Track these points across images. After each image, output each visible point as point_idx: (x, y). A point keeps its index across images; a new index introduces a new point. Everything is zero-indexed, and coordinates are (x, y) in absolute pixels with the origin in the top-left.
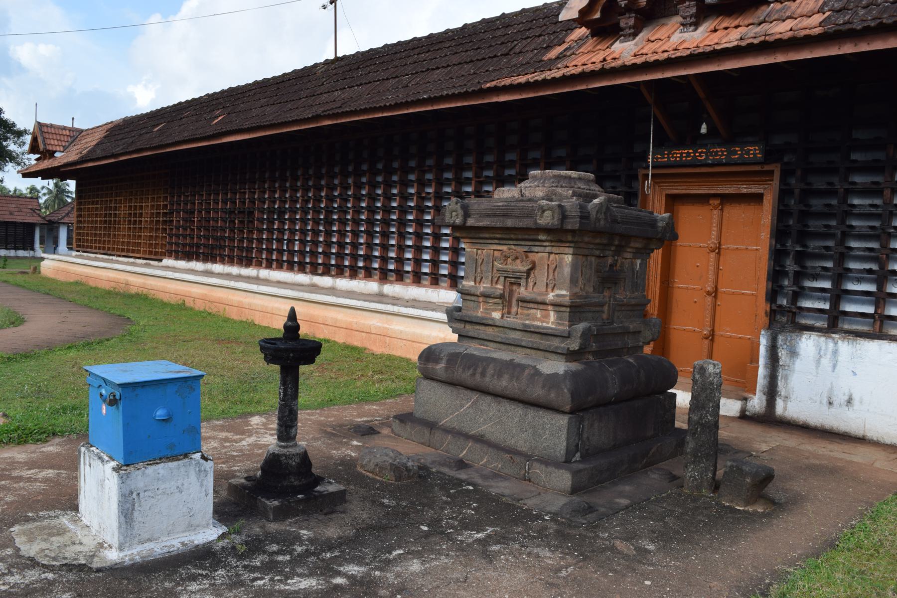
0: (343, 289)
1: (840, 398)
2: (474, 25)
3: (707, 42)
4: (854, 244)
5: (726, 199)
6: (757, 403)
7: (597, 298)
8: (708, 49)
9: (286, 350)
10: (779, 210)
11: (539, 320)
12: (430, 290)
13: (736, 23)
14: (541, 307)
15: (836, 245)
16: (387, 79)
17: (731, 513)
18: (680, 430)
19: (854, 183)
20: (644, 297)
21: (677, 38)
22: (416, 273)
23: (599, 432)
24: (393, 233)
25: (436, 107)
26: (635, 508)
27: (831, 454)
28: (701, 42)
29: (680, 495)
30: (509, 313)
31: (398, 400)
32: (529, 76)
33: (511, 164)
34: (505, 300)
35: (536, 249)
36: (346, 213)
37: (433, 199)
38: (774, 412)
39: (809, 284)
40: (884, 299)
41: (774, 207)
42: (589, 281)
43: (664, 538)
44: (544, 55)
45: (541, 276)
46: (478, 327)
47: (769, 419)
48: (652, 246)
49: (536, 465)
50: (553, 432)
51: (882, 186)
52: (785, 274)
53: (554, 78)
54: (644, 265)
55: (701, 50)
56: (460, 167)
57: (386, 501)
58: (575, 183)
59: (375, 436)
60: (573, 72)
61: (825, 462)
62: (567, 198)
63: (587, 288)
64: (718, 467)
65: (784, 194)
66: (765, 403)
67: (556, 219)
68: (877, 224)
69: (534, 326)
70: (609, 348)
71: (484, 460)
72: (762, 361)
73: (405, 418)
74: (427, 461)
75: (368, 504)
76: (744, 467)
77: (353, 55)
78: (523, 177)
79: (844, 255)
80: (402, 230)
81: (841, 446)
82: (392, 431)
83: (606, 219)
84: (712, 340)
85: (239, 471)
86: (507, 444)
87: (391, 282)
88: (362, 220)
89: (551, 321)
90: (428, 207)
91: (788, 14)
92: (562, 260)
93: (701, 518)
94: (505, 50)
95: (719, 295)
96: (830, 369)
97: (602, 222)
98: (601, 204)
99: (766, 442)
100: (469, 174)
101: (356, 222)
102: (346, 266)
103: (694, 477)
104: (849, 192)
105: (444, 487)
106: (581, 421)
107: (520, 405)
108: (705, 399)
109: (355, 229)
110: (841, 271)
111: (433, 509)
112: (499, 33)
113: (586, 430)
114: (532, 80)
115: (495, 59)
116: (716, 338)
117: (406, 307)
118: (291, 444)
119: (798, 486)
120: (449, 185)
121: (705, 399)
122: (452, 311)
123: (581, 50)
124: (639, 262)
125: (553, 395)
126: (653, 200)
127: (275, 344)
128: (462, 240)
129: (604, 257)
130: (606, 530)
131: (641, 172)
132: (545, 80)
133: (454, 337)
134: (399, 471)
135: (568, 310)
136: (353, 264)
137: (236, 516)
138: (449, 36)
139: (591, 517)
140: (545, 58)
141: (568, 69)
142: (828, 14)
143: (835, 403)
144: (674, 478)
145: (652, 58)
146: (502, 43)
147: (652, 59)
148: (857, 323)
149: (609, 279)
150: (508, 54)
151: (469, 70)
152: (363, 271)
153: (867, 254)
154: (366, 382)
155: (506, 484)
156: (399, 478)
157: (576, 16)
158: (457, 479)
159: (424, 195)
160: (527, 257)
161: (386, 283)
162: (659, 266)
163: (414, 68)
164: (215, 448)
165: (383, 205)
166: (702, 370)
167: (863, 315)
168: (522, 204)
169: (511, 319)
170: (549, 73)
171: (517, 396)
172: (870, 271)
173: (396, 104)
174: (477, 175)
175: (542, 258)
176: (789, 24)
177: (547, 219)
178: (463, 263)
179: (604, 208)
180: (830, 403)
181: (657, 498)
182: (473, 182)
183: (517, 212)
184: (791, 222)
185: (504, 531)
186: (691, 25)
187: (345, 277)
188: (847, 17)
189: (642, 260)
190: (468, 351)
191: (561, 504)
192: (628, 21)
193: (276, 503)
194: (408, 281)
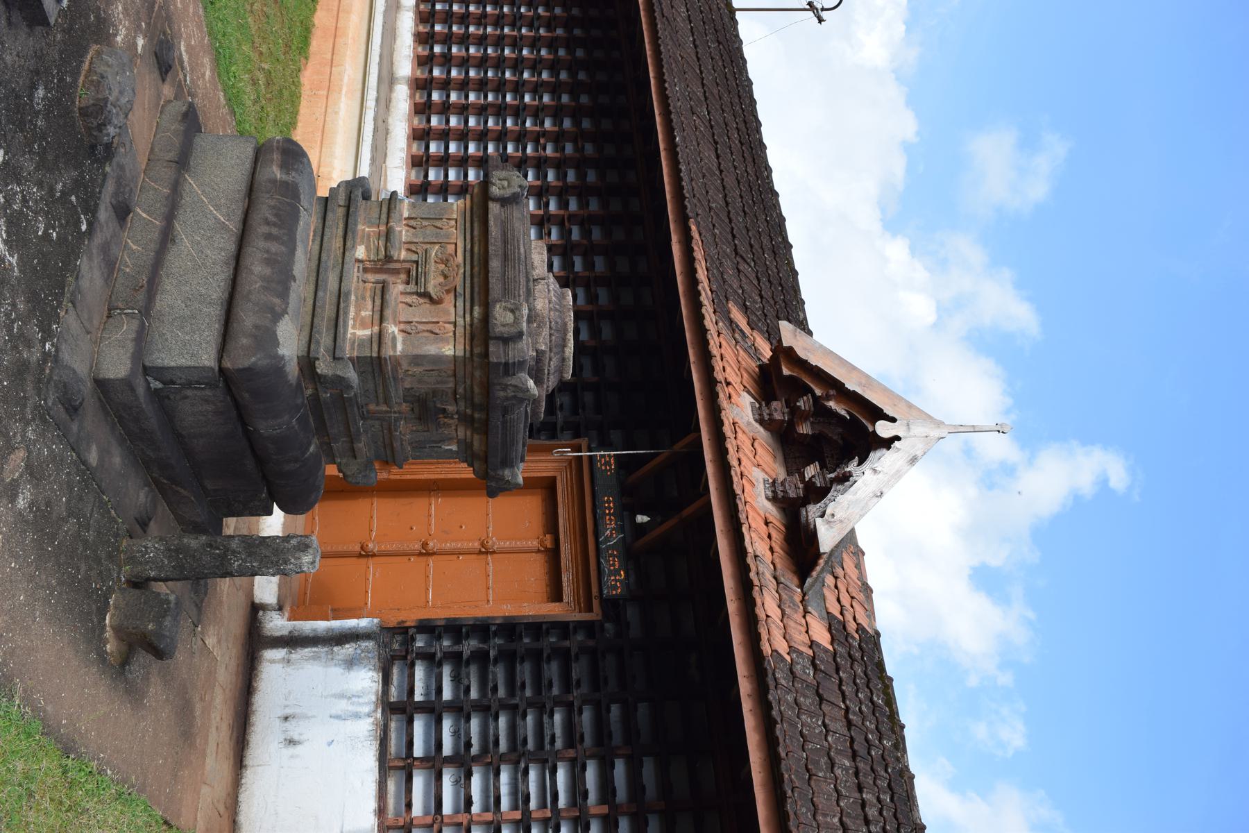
0: (399, 23)
1: (294, 729)
2: (776, 206)
3: (751, 514)
4: (503, 721)
5: (553, 556)
6: (277, 624)
7: (396, 394)
8: (742, 517)
10: (542, 623)
12: (403, 155)
13: (777, 548)
14: (377, 316)
15: (500, 700)
16: (703, 85)
17: (98, 608)
18: (218, 527)
19: (580, 713)
20: (406, 459)
21: (758, 475)
22: (428, 134)
23: (198, 412)
24: (486, 97)
25: (663, 154)
26: (84, 474)
27: (213, 730)
28: (752, 507)
29: (116, 535)
30: (365, 270)
31: (225, 110)
32: (706, 283)
34: (384, 263)
35: (460, 303)
36: (513, 25)
37: (536, 154)
38: (266, 648)
39: (446, 671)
40: (433, 766)
41: (544, 616)
42: (420, 381)
43: (41, 520)
44: (736, 303)
45: (421, 313)
46: (341, 226)
47: (255, 641)
48: (476, 465)
49: (135, 324)
50: (189, 345)
51: (579, 747)
52: (458, 640)
53: (703, 317)
54: (450, 455)
55: (741, 507)
56: (583, 192)
57: (41, 92)
58: (556, 353)
59: (156, 75)
60: (712, 342)
61: (198, 722)
64: (170, 583)
65: (563, 628)
66: (278, 634)
67: (502, 329)
68: (531, 745)
69: (347, 307)
70: (326, 417)
71: (135, 246)
72: (336, 624)
73: (191, 121)
74: (121, 157)
75: (31, 64)
76: (169, 618)
77: (737, 36)
78: (564, 282)
79: (486, 710)
80: (490, 110)
81: (227, 740)
82: (170, 101)
83: (507, 399)
84: (360, 556)
86: (164, 278)
87: (412, 96)
88: (503, 50)
89: (357, 331)
90: (525, 149)
91: (788, 611)
93: (83, 568)
94: (742, 249)
95: (424, 559)
96: (334, 712)
97: (502, 394)
98: (528, 390)
99: (219, 642)
100: (573, 206)
101: (499, 42)
102: (433, 27)
103: (147, 553)
104: (569, 707)
105: (78, 184)
106: (211, 385)
107: (226, 295)
108: (270, 555)
109: (489, 40)
110: (494, 707)
111: (37, 169)
112: (765, 241)
113: (199, 393)
114: (700, 288)
115: (730, 236)
116: (363, 561)
117: (375, 119)
119: (156, 692)
120: (558, 178)
121: (270, 555)
122: (363, 186)
123: (741, 352)
124: (454, 448)
125: (244, 341)
130: (41, 434)
131: (584, 442)
132: (700, 305)
133: (323, 192)
134: (97, 112)
135: (375, 355)
136: (437, 38)
138: (762, 173)
139: (60, 411)
140: (731, 305)
141: (715, 336)
142: (788, 658)
143: (287, 724)
144: (143, 524)
145: (730, 445)
146: (751, 246)
147: (729, 446)
148: (399, 738)
149: (425, 409)
150: (737, 254)
151: (715, 201)
152: (426, 53)
153: (491, 738)
154: (250, 60)
155: (99, 282)
156: (84, 112)
157: (785, 344)
158: (96, 205)
159: (542, 141)
160: (448, 292)
161: (410, 88)
162: (457, 476)
163: (717, 123)
165: (525, 82)
166: (304, 547)
167: (410, 744)
168: (523, 280)
169: (356, 274)
170: (711, 310)
171: (239, 289)
172: (468, 745)
173: (667, 97)
174: (572, 218)
175: (447, 313)
176: (774, 612)
177: (501, 316)
179: (521, 396)
180: (286, 718)
181: (106, 504)
182: (562, 212)
183: (510, 274)
184: (526, 640)
185: (13, 281)
186: (774, 492)
187: (417, 25)
188: (783, 682)
189: (457, 452)
190: (303, 213)
191: (75, 366)
192: (778, 410)
194: (416, 121)
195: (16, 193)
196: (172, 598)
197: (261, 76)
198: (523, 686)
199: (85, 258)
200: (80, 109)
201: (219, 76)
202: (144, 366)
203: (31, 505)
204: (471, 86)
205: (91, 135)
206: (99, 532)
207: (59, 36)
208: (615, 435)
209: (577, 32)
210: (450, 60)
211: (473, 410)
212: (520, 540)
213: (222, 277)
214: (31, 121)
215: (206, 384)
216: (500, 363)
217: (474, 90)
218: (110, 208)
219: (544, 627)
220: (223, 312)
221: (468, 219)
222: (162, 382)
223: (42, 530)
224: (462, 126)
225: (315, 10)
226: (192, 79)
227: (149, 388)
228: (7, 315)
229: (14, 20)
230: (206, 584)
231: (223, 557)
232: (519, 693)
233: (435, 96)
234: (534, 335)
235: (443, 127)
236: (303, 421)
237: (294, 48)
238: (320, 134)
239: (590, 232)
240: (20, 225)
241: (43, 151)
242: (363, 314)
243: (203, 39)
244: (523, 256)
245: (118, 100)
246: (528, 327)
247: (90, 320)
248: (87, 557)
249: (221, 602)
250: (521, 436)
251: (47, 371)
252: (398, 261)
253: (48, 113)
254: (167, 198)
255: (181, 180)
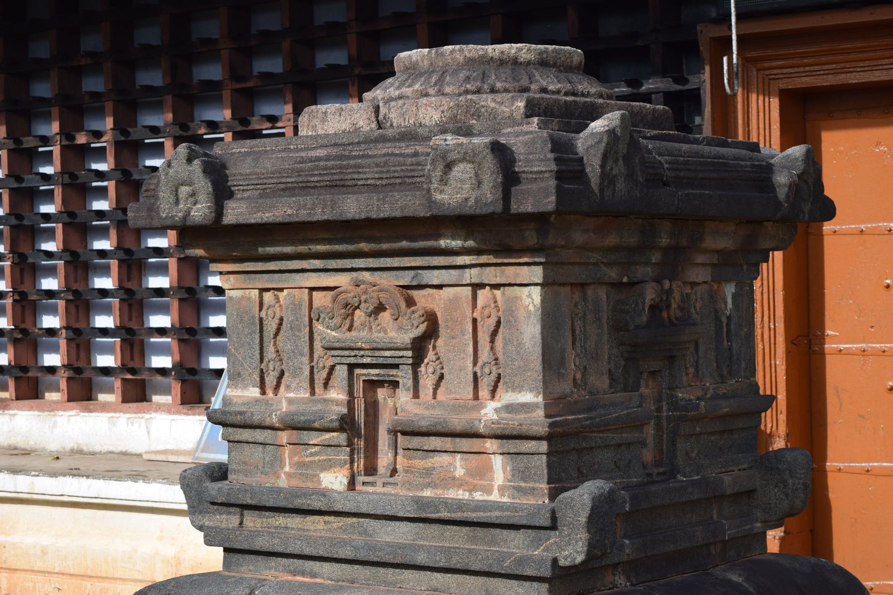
11: (459, 483)
14: (465, 444)
30: (371, 470)
33: (334, 34)
34: (357, 431)
35: (435, 277)
45: (453, 351)
54: (745, 298)
62: (514, 123)
63: (592, 379)
67: (487, 186)
69: (446, 504)
78: (369, 72)
89: (496, 482)
92: (512, 304)
100: (213, 72)
117: (54, 474)
126: (747, 112)
128: (214, 267)
129: (631, 284)
131: (707, 33)
133: (213, 558)
135: (544, 446)
159: (81, 139)
168: (382, 149)
174: (237, 73)
175: (454, 302)
177: (463, 188)
178: (219, 332)
182: (227, 94)
183: (370, 175)
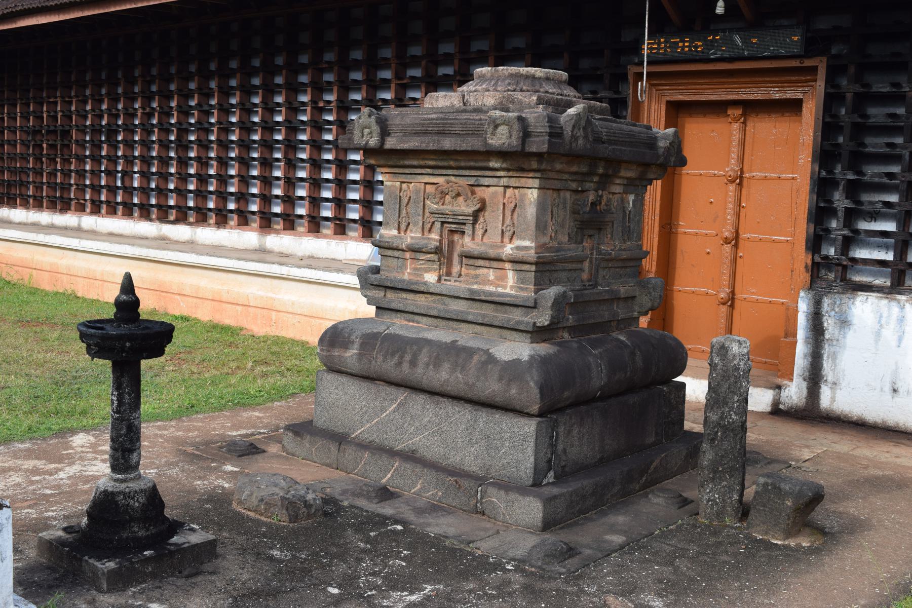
0: (207, 242)
5: (751, 108)
7: (574, 250)
9: (119, 338)
10: (824, 123)
15: (903, 171)
23: (580, 440)
24: (278, 160)
26: (633, 548)
27: (898, 461)
29: (694, 526)
30: (449, 274)
31: (291, 402)
34: (442, 255)
35: (486, 181)
36: (208, 131)
38: (818, 404)
39: (864, 225)
41: (817, 119)
45: (493, 220)
46: (404, 295)
47: (811, 414)
49: (492, 491)
50: (516, 443)
52: (833, 212)
57: (276, 553)
59: (259, 457)
64: (747, 484)
65: (831, 100)
66: (805, 392)
67: (514, 138)
69: (484, 292)
70: (592, 321)
71: (419, 486)
73: (301, 429)
74: (335, 491)
75: (250, 558)
76: (782, 485)
80: (291, 156)
82: (283, 446)
83: (586, 137)
84: (732, 306)
85: (55, 518)
86: (449, 462)
87: (277, 232)
88: (232, 142)
89: (509, 284)
93: (724, 558)
95: (741, 243)
96: (894, 343)
97: (581, 142)
98: (578, 115)
99: (808, 447)
100: (387, 74)
101: (224, 145)
102: (210, 210)
103: (714, 500)
106: (554, 426)
107: (467, 406)
109: (223, 155)
113: (561, 438)
117: (299, 267)
118: (132, 476)
119: (854, 508)
120: (359, 90)
121: (727, 389)
122: (366, 273)
125: (513, 391)
127: (102, 329)
130: (593, 581)
131: (632, 70)
133: (371, 311)
134: (295, 507)
135: (533, 268)
136: (221, 206)
137: (50, 587)
139: (572, 563)
143: (901, 390)
144: (685, 502)
149: (590, 223)
152: (235, 217)
154: (243, 377)
155: (450, 519)
156: (294, 518)
158: (379, 515)
159: (321, 104)
160: (473, 193)
161: (269, 233)
162: (658, 198)
164: (19, 485)
166: (723, 350)
168: (465, 116)
169: (452, 283)
171: (462, 394)
174: (399, 76)
175: (494, 194)
177: (501, 138)
179: (584, 122)
180: (895, 391)
182: (393, 86)
183: (458, 128)
184: (841, 140)
185: (448, 590)
187: (209, 225)
190: (391, 330)
191: (529, 546)
193: (111, 565)
195: (368, 581)
196: (762, 480)
197: (258, 369)
198: (891, 145)
199: (428, 529)
200: (290, 522)
201: (259, 404)
202: (532, 486)
203: (660, 595)
204: (267, 174)
205: (314, 514)
206: (691, 541)
207: (224, 534)
208: (627, 36)
209: (213, 67)
210: (242, 194)
211: (596, 174)
212: (730, 142)
213: (449, 408)
214: (302, 563)
215: (553, 430)
216: (549, 141)
217: (271, 172)
218: (382, 504)
219: (828, 120)
220: (484, 410)
221: (401, 171)
222: (549, 471)
223: (685, 589)
224: (306, 184)
225: (196, 319)
226: (262, 428)
227: (553, 483)
228: (479, 597)
229: (211, 570)
230: (750, 452)
231: (726, 429)
232: (898, 151)
233: (277, 209)
234: (521, 106)
235: (307, 203)
236: (595, 344)
237: (232, 339)
238: (313, 320)
239: (414, 57)
240: (396, 580)
241: (328, 555)
242: (492, 278)
243: (226, 416)
244: (441, 116)
245: (282, 488)
246: (513, 111)
247: (486, 530)
248: (714, 554)
249: (767, 441)
250: (625, 127)
251: (533, 569)
252: (441, 241)
253: (292, 548)
254: (374, 454)
255: (357, 441)
